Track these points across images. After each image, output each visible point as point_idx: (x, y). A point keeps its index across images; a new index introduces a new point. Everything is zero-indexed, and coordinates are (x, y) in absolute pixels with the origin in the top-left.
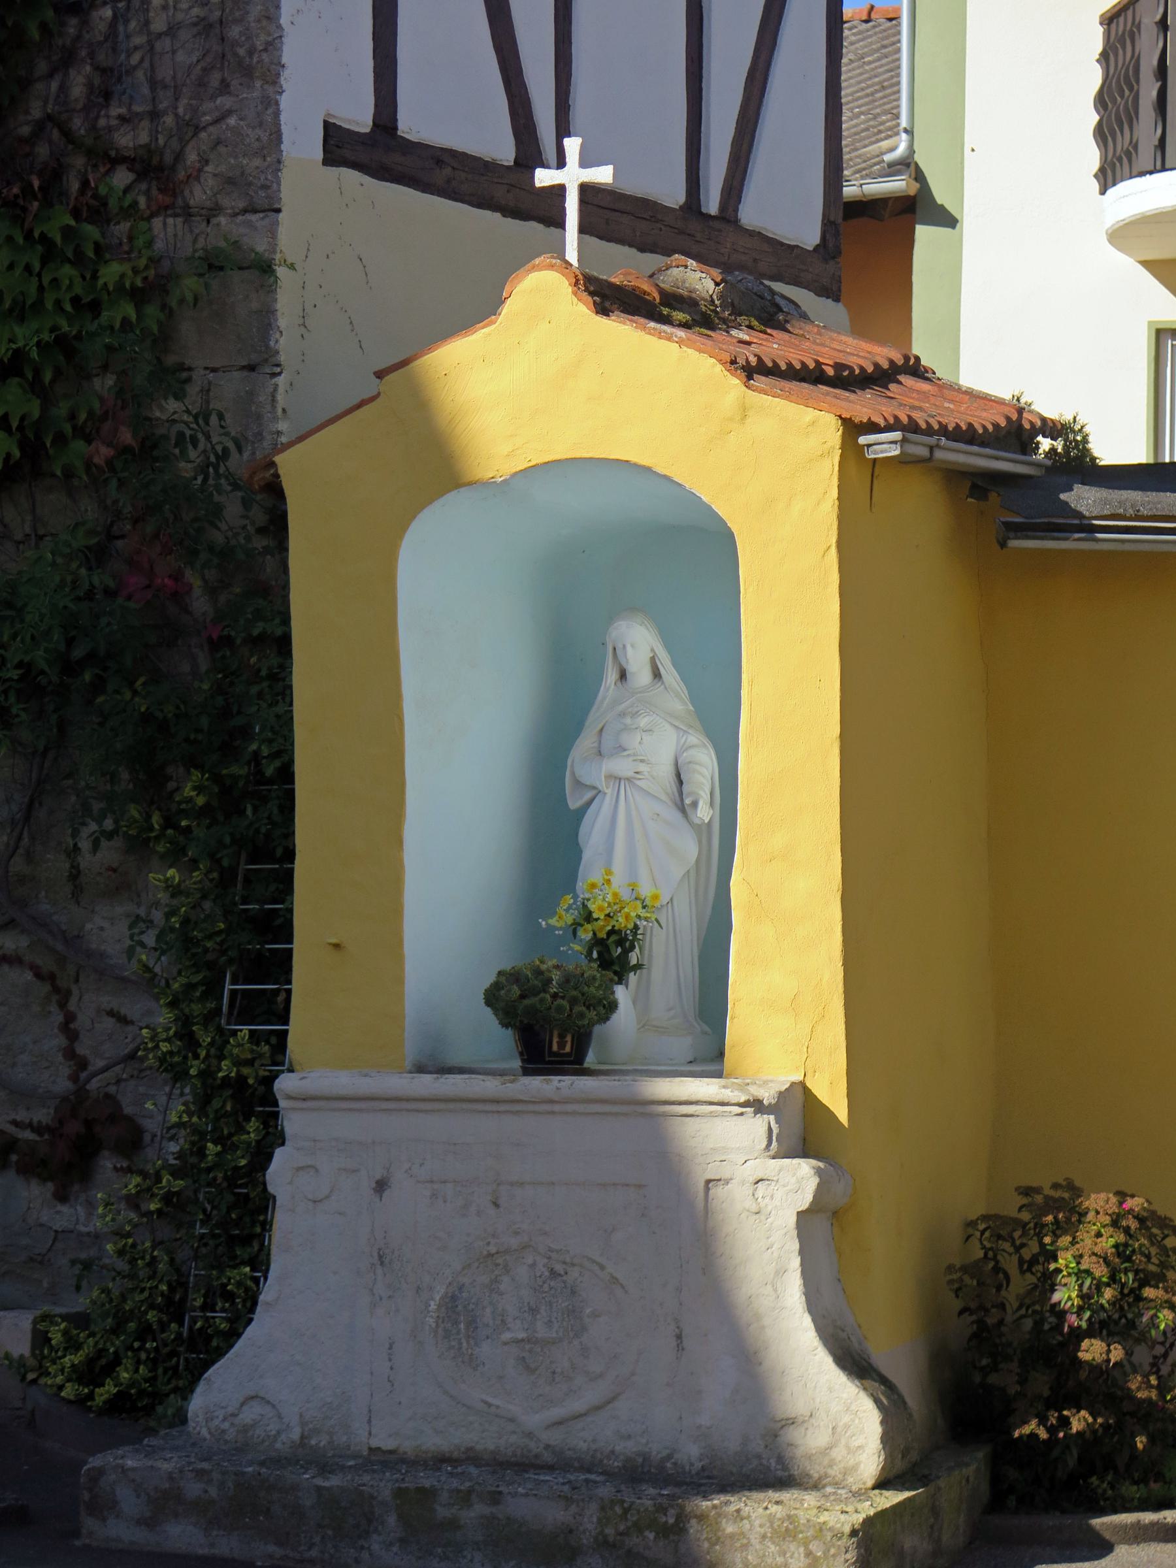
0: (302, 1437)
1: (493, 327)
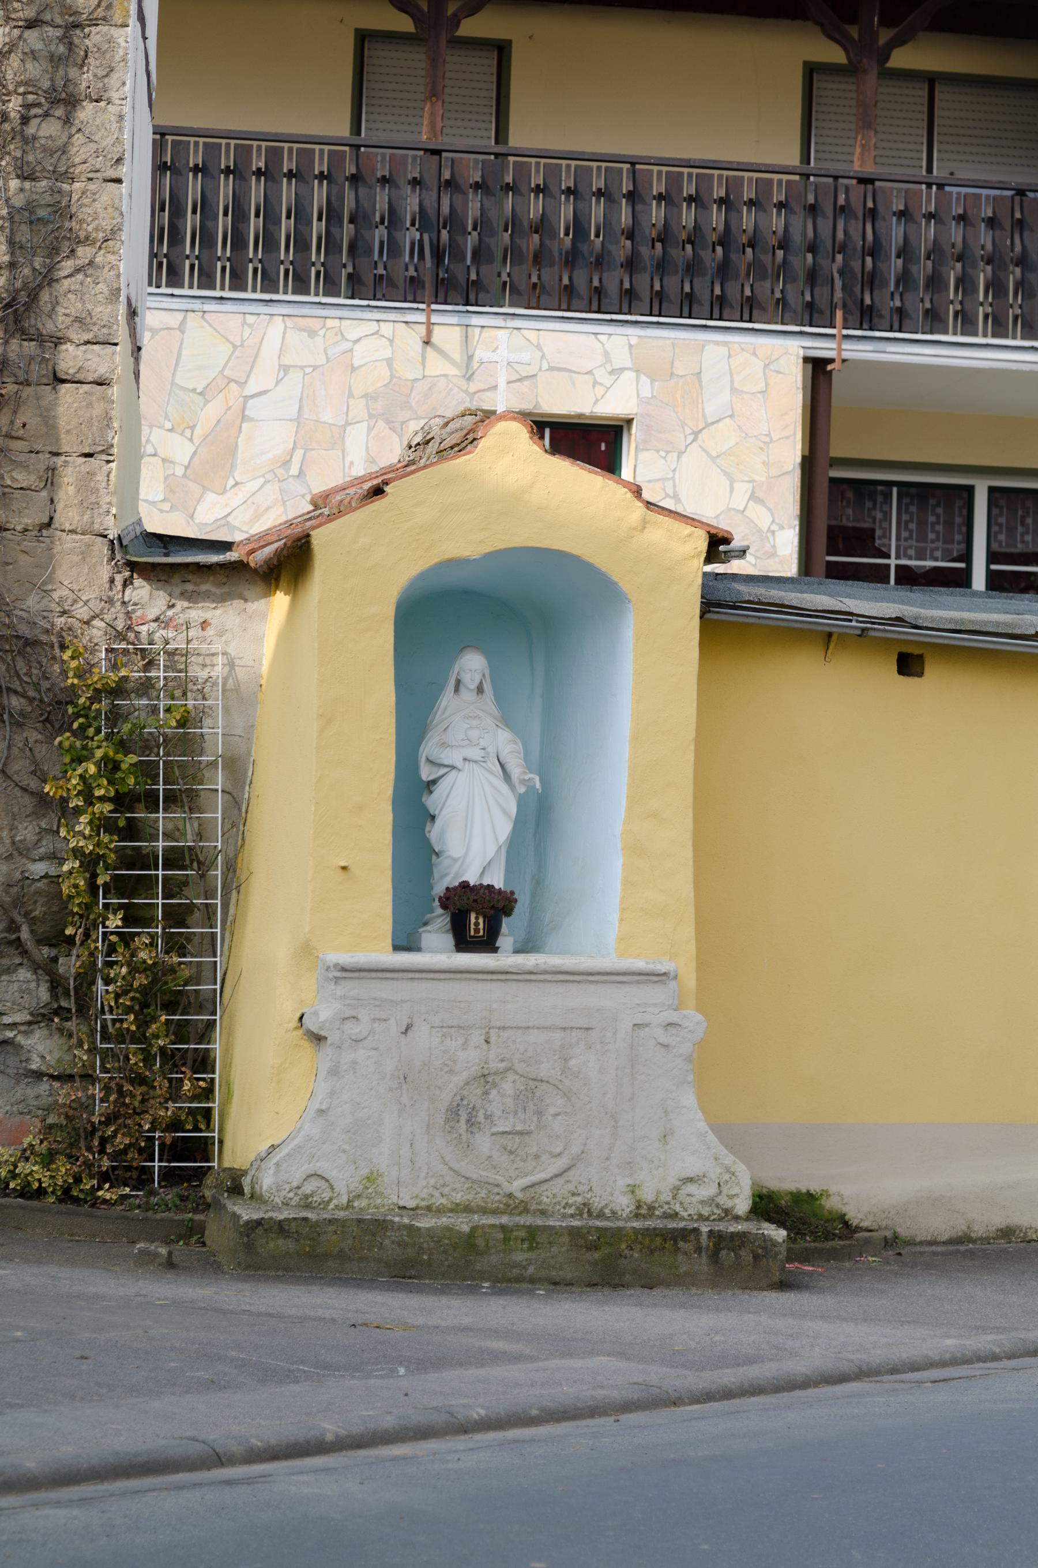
0: (349, 1201)
1: (471, 455)
